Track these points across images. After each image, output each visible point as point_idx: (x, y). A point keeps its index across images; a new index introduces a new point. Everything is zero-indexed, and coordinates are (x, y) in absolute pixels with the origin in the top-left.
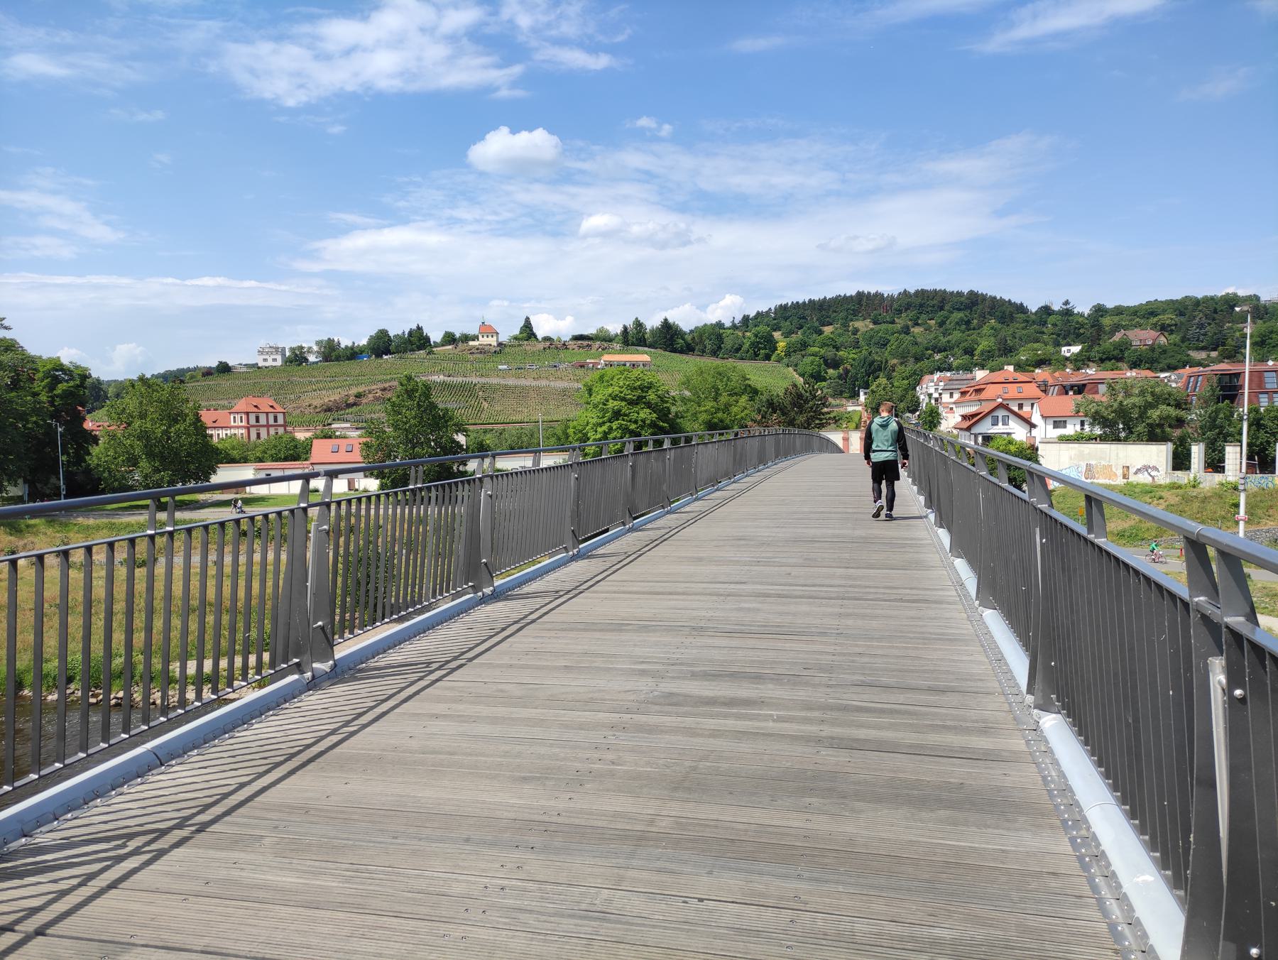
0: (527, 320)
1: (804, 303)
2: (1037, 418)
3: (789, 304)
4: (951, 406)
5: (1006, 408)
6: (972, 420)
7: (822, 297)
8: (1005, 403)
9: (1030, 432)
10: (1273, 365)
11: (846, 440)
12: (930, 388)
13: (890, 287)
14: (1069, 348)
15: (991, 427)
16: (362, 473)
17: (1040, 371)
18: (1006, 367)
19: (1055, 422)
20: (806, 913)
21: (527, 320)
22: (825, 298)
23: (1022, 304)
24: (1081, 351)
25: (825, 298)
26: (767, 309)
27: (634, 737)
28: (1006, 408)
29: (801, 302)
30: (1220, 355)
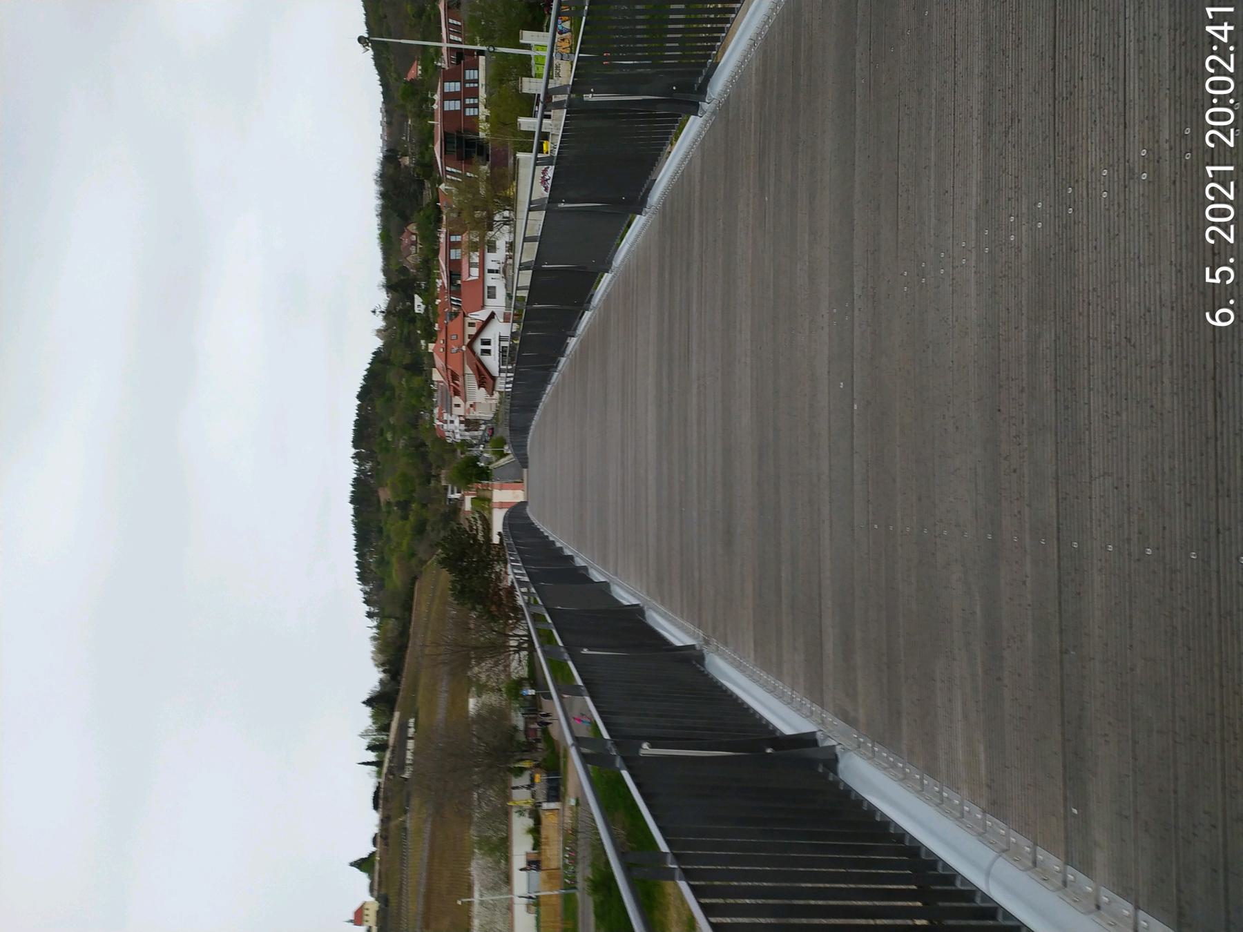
0: (353, 864)
1: (357, 555)
2: (482, 315)
3: (358, 570)
4: (468, 406)
5: (473, 338)
6: (485, 379)
7: (353, 538)
8: (467, 340)
9: (521, 904)
10: (437, 104)
11: (502, 505)
12: (453, 428)
13: (348, 470)
14: (416, 306)
15: (492, 356)
16: (550, 80)
17: (437, 325)
18: (430, 351)
19: (489, 297)
20: (1127, 149)
21: (353, 864)
22: (354, 535)
23: (373, 354)
24: (467, 711)
25: (354, 535)
26: (362, 593)
27: (1059, 115)
28: (473, 338)
29: (356, 559)
30: (428, 179)
